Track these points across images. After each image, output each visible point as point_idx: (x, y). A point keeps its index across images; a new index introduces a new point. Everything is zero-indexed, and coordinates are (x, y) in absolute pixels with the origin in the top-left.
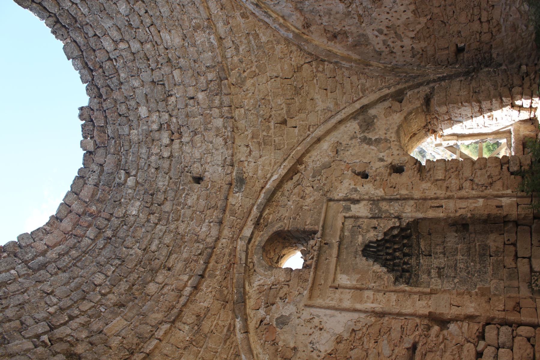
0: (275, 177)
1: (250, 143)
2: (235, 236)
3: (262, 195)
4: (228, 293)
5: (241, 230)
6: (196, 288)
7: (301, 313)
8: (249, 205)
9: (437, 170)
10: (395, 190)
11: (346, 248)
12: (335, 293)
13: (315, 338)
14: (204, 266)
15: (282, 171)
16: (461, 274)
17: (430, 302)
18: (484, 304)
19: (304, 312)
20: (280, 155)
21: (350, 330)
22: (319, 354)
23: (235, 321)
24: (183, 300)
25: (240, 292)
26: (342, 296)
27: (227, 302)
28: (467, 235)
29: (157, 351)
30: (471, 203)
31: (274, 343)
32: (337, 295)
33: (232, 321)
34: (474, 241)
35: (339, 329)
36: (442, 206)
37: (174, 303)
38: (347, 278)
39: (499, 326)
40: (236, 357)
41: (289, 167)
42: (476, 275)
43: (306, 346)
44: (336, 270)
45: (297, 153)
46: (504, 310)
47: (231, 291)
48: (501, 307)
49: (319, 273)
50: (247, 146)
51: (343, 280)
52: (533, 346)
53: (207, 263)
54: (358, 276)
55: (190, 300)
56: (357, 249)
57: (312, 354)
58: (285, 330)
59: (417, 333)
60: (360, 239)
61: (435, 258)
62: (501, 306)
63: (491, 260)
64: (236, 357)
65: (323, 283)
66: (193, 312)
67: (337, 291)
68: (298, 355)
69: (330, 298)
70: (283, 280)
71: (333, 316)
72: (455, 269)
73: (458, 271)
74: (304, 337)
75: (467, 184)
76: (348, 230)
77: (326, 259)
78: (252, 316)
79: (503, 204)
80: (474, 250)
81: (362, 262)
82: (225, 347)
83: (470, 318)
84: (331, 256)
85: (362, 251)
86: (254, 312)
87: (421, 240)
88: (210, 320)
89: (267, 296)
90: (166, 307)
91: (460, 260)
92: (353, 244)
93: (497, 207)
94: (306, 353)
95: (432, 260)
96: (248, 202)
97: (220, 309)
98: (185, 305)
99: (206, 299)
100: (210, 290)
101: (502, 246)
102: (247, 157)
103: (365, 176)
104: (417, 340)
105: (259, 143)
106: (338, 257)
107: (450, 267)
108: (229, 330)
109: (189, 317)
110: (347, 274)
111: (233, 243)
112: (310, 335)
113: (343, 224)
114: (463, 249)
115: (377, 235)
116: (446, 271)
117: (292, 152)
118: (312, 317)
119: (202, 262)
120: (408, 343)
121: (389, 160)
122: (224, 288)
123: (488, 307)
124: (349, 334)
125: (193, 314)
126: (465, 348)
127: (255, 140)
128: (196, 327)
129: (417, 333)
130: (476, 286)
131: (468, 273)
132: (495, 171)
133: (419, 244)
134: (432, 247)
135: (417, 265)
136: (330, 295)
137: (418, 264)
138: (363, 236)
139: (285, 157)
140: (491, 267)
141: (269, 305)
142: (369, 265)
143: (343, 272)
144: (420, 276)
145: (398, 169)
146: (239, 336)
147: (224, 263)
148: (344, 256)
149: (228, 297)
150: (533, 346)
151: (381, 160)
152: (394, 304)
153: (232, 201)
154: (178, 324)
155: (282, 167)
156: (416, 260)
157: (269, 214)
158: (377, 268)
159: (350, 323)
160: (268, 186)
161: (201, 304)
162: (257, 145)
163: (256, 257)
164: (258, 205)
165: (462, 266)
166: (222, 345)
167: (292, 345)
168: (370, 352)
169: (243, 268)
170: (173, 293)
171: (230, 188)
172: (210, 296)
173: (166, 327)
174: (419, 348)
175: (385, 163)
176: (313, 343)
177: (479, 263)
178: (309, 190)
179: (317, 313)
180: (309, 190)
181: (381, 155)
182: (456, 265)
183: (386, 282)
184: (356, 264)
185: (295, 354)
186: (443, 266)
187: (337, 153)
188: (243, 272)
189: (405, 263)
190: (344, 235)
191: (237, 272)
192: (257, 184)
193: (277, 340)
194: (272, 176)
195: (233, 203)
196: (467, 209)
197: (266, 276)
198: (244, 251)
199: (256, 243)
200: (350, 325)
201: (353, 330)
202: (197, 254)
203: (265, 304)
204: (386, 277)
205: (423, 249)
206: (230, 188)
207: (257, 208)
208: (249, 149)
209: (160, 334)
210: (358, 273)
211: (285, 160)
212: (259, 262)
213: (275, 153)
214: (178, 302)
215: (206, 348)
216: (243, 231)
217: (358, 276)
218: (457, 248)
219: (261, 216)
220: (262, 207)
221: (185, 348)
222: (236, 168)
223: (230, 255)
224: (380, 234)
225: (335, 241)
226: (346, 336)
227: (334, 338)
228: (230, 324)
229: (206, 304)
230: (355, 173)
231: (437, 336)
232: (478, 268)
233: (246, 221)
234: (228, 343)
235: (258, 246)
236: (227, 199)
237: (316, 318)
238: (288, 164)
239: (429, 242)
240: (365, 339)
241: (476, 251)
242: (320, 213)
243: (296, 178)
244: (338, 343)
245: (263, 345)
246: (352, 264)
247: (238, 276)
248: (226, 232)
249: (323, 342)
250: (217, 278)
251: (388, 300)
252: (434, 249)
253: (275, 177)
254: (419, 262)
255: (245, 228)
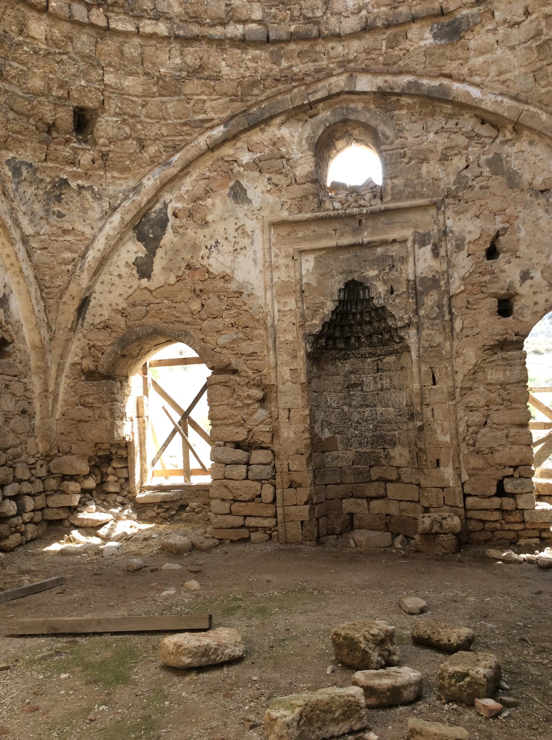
0: (475, 92)
1: (534, 16)
2: (352, 65)
3: (435, 83)
4: (257, 95)
5: (366, 71)
6: (243, 42)
7: (252, 217)
8: (413, 65)
9: (505, 370)
10: (464, 309)
11: (356, 256)
12: (287, 256)
13: (224, 247)
14: (285, 37)
15: (488, 100)
16: (355, 414)
17: (290, 384)
18: (294, 448)
19: (255, 220)
20: (522, 83)
21: (241, 290)
22: (205, 258)
23: (218, 125)
24: (217, 32)
25: (263, 114)
26: (283, 269)
27: (242, 101)
28: (405, 420)
29: (121, 39)
30: (442, 425)
31: (208, 192)
32: (284, 261)
33: (217, 121)
34: (399, 428)
35: (240, 276)
36: (434, 384)
37: (208, 21)
38: (311, 269)
39: (272, 465)
40: (172, 147)
41: (500, 111)
42: (356, 432)
43: (211, 238)
44: (320, 250)
45: (533, 116)
46: (289, 470)
47: (260, 98)
48: (294, 467)
49: (313, 227)
50: (527, 13)
51: (308, 263)
52: (253, 500)
53: (294, 37)
54: (314, 283)
55: (219, 43)
56: (355, 271)
57: (203, 248)
58: (228, 201)
59: (250, 373)
60: (372, 273)
61: (375, 378)
62: (295, 467)
63: (378, 451)
64: (172, 147)
65: (300, 236)
66: (205, 57)
67: (290, 259)
68: (199, 231)
69: (278, 252)
70: (297, 174)
71: (255, 263)
72: (362, 406)
73: (360, 410)
74: (222, 231)
75: (477, 417)
76: (385, 252)
77: (335, 230)
78: (239, 144)
79: (442, 468)
80: (389, 428)
81: (336, 284)
82: (178, 127)
83: (274, 433)
84: (341, 235)
85: (353, 281)
86: (245, 146)
87: (394, 357)
88: (204, 89)
89: (271, 158)
90: (195, 12)
91: (375, 410)
92: (363, 264)
93: (438, 461)
94: (204, 239)
95: (371, 374)
96: (416, 61)
97: (228, 96)
98: (210, 40)
99: (231, 66)
100: (251, 65)
101: (396, 465)
102: (505, 21)
103: (492, 253)
104: (242, 374)
105: (539, 33)
106: (339, 248)
107: (364, 398)
108: (203, 121)
109: (193, 55)
110: (315, 268)
111: (340, 67)
112: (226, 238)
113: (394, 241)
114: (389, 414)
115: (380, 297)
116: (358, 393)
117: (535, 106)
118: (250, 234)
119: (292, 28)
120: (235, 362)
121: (524, 289)
122: (262, 86)
123: (291, 453)
124: (236, 289)
125: (201, 59)
126: (240, 430)
127: (543, 24)
128: (184, 74)
129: (250, 373)
130: (338, 433)
131: (358, 422)
132: (506, 454)
133: (390, 354)
134: (387, 373)
135: (362, 355)
136: (283, 251)
137: (364, 357)
138: (378, 276)
139: (523, 96)
140: (369, 450)
141: (257, 166)
142: (332, 295)
143: (317, 261)
144: (348, 361)
145: (505, 307)
146: (202, 141)
147: (302, 66)
148: (343, 256)
149: (249, 98)
150: (253, 500)
151: (525, 276)
152: (282, 339)
153: (414, 30)
154: (176, 46)
155: (499, 98)
156: (369, 353)
157: (409, 106)
158: (330, 306)
159: (250, 287)
160: (456, 86)
161: (223, 64)
162: (533, 33)
163: (329, 113)
164: (416, 82)
165: (366, 414)
166: (179, 121)
167: (210, 218)
168: (219, 320)
169: (300, 103)
170: (223, 7)
171: (436, 16)
172: (242, 71)
173: (162, 28)
174: (233, 377)
175: (517, 284)
176: (217, 246)
177: (373, 436)
178: (459, 162)
179: (256, 241)
180: (459, 162)
181: (536, 274)
182: (367, 406)
183: (310, 323)
184: (332, 277)
185: (200, 225)
186: (365, 389)
187: (542, 192)
188: (295, 105)
189: (358, 339)
190: (376, 246)
191: (296, 96)
192: (455, 64)
193: (212, 194)
194: (477, 85)
195: (409, 36)
196: (431, 419)
197: (300, 143)
198: (329, 91)
199: (352, 105)
200: (247, 288)
201: (241, 293)
202: (304, 11)
203: (259, 158)
204: (317, 322)
205: (384, 361)
206: (436, 16)
207: (410, 82)
208: (523, 18)
209: (148, 27)
210: (319, 283)
211: (516, 98)
212: (322, 122)
213: (526, 73)
214: (212, 26)
215: (163, 103)
216: (364, 75)
217: (314, 283)
218: (389, 406)
219: (399, 94)
220: (413, 91)
221: (146, 74)
222: (475, 10)
223: (318, 71)
224: (381, 301)
225: (366, 237)
226: (233, 286)
227: (228, 271)
228: (212, 119)
229: (225, 71)
230: (497, 235)
231: (249, 397)
232: (367, 434)
233: (381, 73)
234: (185, 128)
235: (348, 109)
236: (414, 19)
237: (250, 241)
238: (505, 106)
239: (393, 369)
240: (233, 311)
241: (388, 431)
242: (414, 197)
243: (484, 131)
244: (223, 277)
245: (204, 177)
246: (332, 270)
247: (287, 100)
248: (356, 45)
249: (221, 259)
250: (274, 67)
251: (285, 330)
252: (386, 375)
253: (475, 92)
254: (366, 358)
255: (369, 77)
